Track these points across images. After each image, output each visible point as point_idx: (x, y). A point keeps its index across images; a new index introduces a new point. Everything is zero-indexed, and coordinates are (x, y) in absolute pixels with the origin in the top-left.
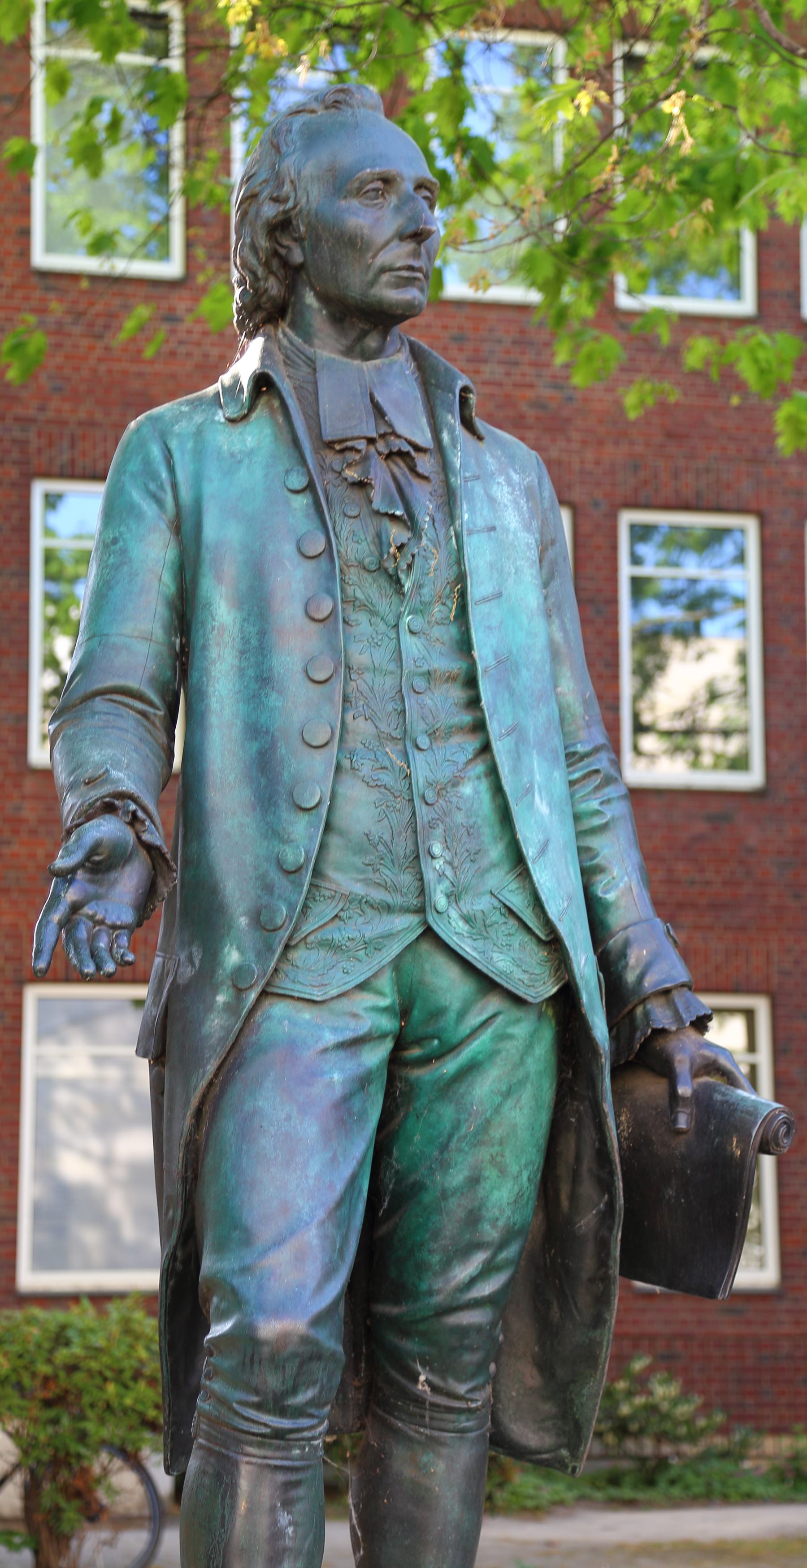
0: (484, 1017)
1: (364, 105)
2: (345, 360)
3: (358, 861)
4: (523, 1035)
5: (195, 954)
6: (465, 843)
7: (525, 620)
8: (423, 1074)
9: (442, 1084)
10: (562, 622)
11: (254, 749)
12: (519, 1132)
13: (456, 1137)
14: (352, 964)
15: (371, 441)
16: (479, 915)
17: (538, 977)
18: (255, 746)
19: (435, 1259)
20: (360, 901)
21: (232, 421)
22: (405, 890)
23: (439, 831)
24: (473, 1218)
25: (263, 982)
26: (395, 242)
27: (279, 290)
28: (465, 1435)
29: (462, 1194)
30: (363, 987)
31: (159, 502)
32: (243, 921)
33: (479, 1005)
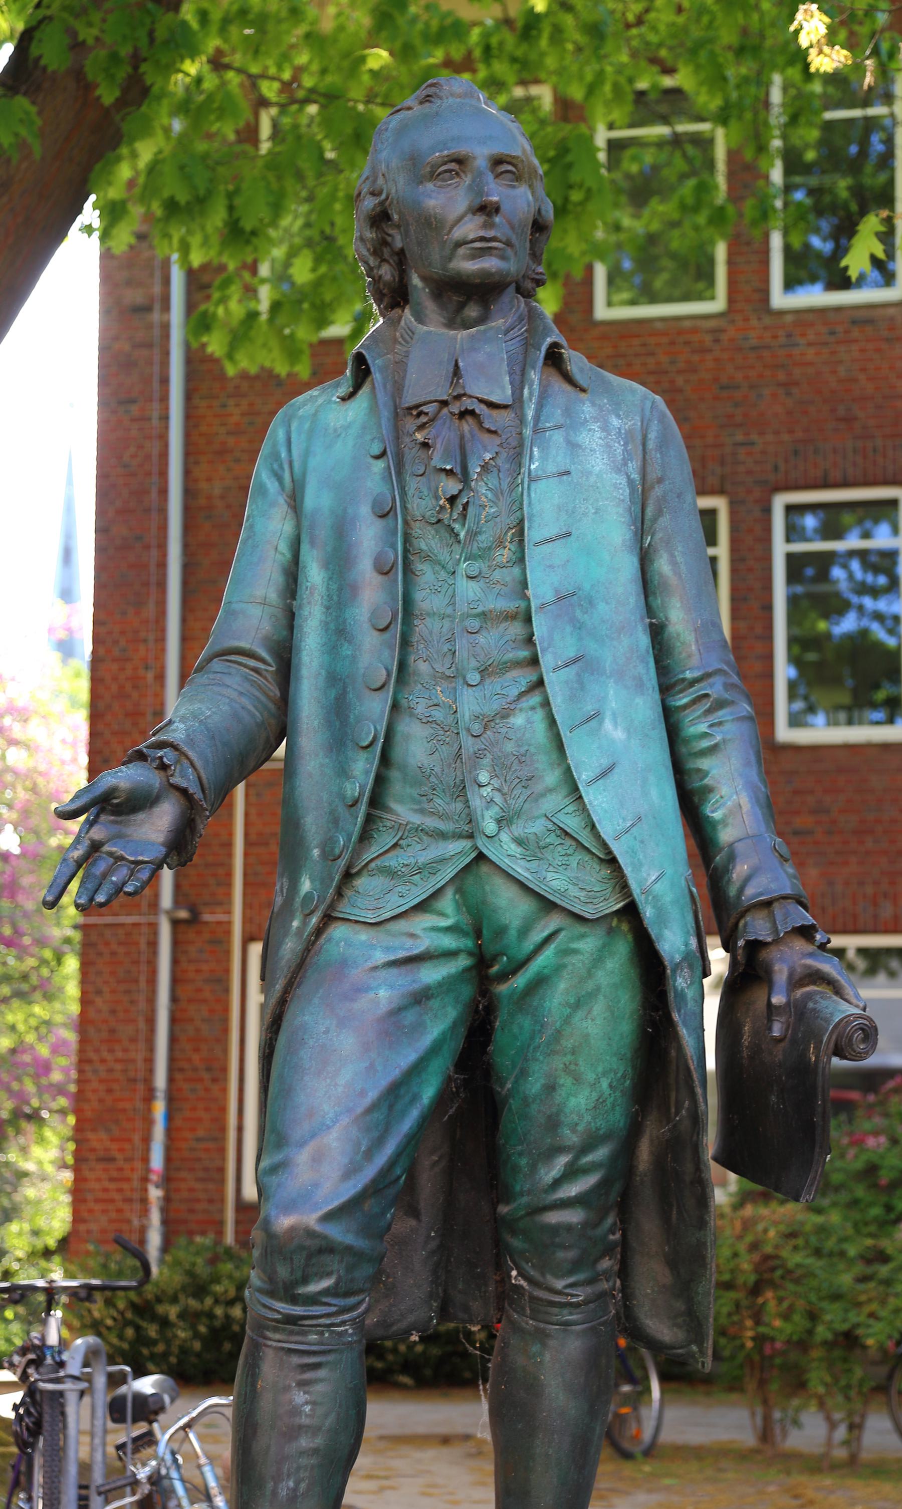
0: (546, 933)
1: (452, 95)
2: (445, 331)
3: (414, 792)
4: (306, 1078)
5: (285, 884)
6: (516, 770)
8: (503, 989)
9: (515, 997)
10: (672, 556)
11: (333, 696)
12: (592, 1041)
13: (532, 1048)
14: (407, 888)
15: (444, 403)
16: (532, 837)
17: (598, 894)
18: (333, 693)
19: (523, 1162)
20: (417, 829)
21: (343, 399)
22: (456, 817)
23: (487, 761)
24: (553, 1123)
25: (322, 908)
26: (470, 216)
27: (393, 276)
28: (569, 1328)
29: (541, 1100)
30: (422, 907)
31: (279, 479)
32: (316, 852)
33: (543, 923)
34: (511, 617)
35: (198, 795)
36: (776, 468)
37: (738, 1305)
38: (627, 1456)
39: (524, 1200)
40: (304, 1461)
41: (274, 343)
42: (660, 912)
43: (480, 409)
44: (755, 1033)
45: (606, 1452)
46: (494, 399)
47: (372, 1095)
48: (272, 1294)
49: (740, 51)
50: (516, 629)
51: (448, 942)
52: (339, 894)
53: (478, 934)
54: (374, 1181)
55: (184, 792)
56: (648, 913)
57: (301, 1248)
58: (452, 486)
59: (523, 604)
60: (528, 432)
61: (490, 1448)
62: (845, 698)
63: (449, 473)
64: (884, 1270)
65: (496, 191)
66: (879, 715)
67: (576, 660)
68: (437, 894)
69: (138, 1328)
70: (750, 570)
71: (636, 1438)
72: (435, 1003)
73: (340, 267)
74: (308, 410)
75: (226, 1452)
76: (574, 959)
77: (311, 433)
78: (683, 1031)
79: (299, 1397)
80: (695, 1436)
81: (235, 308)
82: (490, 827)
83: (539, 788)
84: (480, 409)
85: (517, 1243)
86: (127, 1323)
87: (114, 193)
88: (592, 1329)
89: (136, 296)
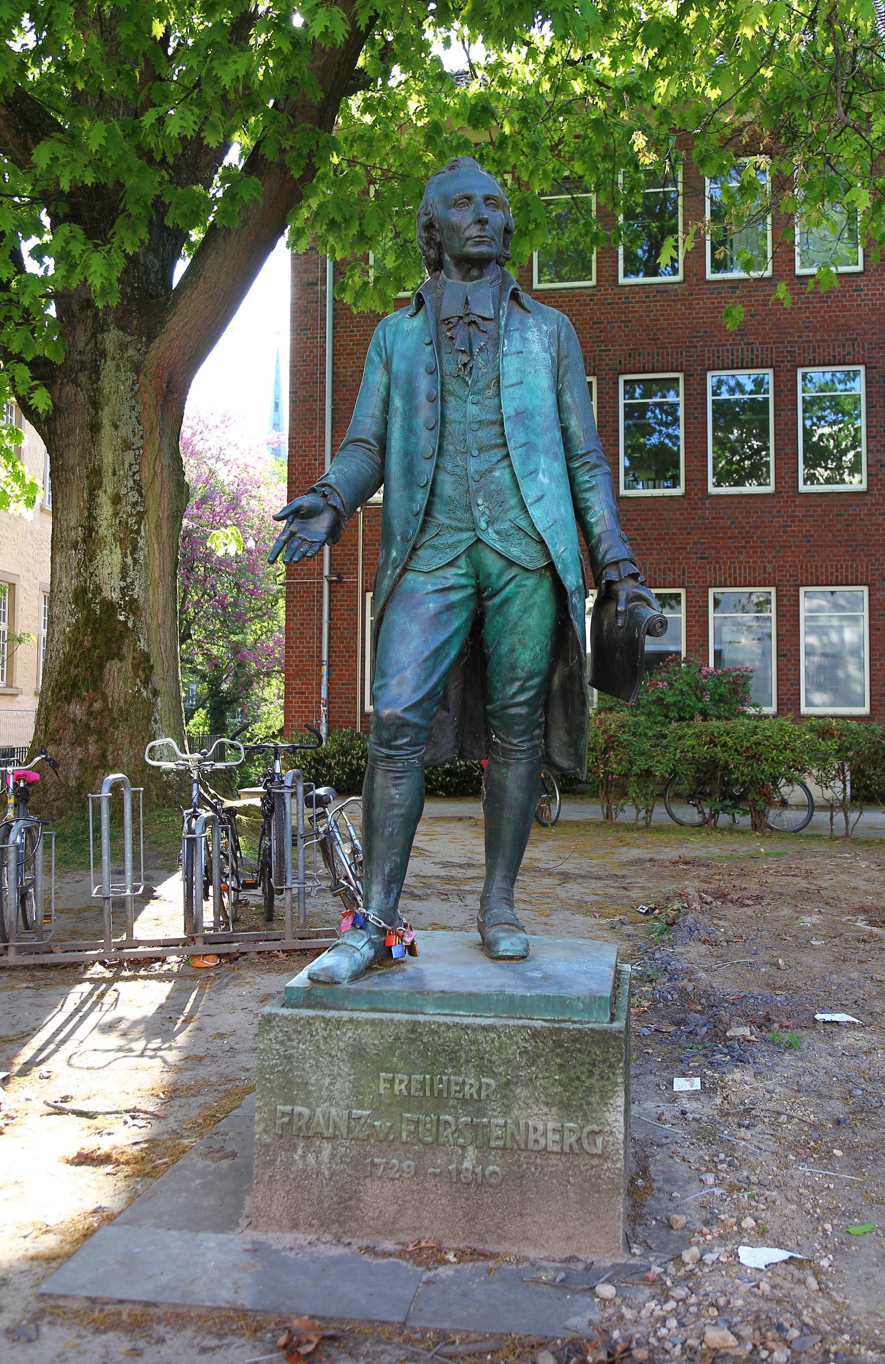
3: (446, 509)
7: (540, 393)
8: (489, 603)
15: (461, 318)
18: (406, 461)
19: (499, 685)
23: (481, 493)
24: (513, 667)
30: (450, 564)
31: (380, 355)
34: (493, 423)
35: (342, 510)
36: (620, 362)
37: (597, 759)
38: (544, 825)
39: (499, 703)
40: (396, 820)
41: (376, 297)
42: (565, 567)
43: (478, 320)
44: (610, 625)
45: (535, 824)
46: (485, 315)
47: (426, 653)
48: (380, 745)
49: (604, 158)
50: (496, 429)
51: (463, 581)
52: (410, 558)
53: (477, 577)
54: (428, 694)
55: (335, 508)
56: (559, 567)
57: (394, 724)
58: (465, 358)
59: (499, 417)
60: (502, 332)
61: (482, 823)
62: (653, 476)
63: (463, 352)
64: (665, 742)
65: (486, 214)
66: (669, 484)
67: (525, 444)
68: (457, 558)
69: (317, 769)
70: (607, 412)
71: (549, 817)
72: (457, 610)
73: (408, 260)
74: (394, 321)
75: (360, 821)
76: (523, 589)
77: (395, 332)
78: (575, 623)
79: (394, 791)
80: (575, 817)
81: (358, 281)
82: (483, 525)
83: (507, 506)
84: (478, 320)
85: (495, 723)
86: (313, 767)
87: (299, 224)
88: (531, 762)
89: (310, 278)
